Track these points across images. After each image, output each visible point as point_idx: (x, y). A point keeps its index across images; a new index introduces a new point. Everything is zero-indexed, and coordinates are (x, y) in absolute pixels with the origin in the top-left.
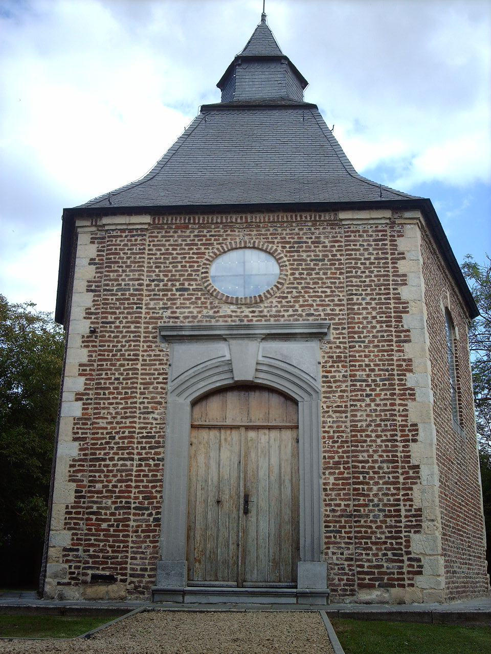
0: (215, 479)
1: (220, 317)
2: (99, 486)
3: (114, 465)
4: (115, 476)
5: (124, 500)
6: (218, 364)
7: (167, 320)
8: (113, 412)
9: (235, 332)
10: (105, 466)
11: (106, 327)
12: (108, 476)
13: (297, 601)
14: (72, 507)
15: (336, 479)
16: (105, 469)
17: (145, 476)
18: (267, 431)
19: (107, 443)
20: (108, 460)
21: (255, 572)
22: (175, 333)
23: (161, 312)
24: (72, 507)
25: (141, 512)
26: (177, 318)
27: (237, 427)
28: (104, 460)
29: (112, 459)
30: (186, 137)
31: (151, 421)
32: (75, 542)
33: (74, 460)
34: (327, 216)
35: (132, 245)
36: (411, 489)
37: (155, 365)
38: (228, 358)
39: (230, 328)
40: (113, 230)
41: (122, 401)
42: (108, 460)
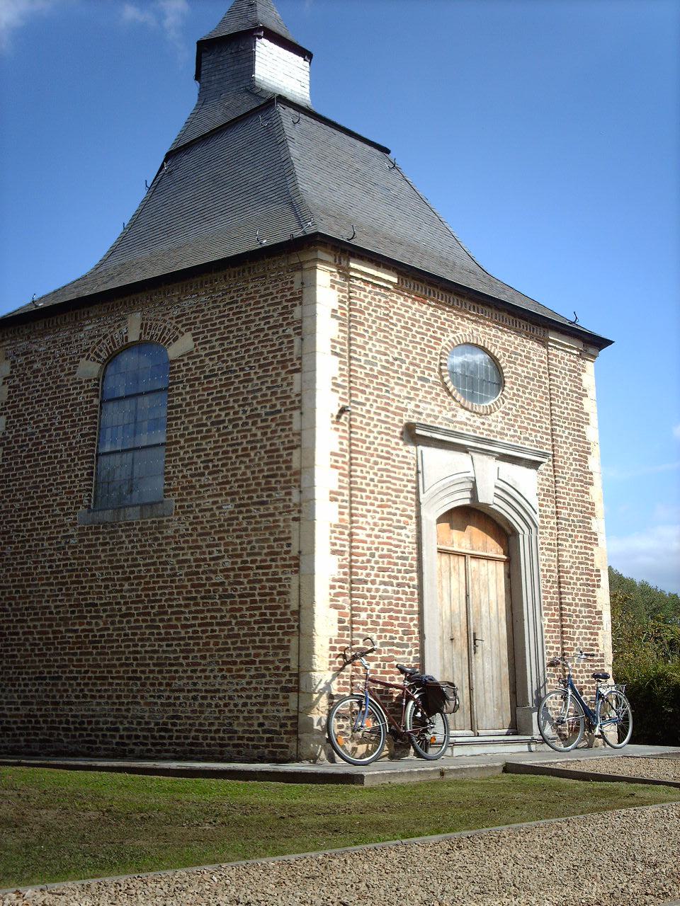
0: (448, 612)
1: (458, 422)
2: (363, 616)
3: (377, 590)
4: (378, 604)
5: (388, 635)
6: (463, 480)
7: (411, 414)
8: (371, 521)
9: (479, 446)
10: (369, 590)
11: (357, 409)
12: (371, 603)
13: (529, 748)
14: (336, 642)
15: (550, 621)
16: (368, 594)
17: (404, 606)
18: (485, 561)
19: (369, 561)
20: (369, 583)
21: (484, 718)
22: (428, 434)
23: (406, 401)
24: (336, 642)
25: (401, 650)
26: (420, 413)
27: (464, 555)
28: (366, 582)
29: (373, 582)
30: (194, 115)
31: (403, 538)
32: (341, 686)
33: (334, 580)
34: (539, 332)
35: (377, 306)
36: (597, 634)
37: (403, 468)
38: (472, 474)
39: (478, 440)
40: (357, 279)
41: (379, 510)
42: (369, 583)
